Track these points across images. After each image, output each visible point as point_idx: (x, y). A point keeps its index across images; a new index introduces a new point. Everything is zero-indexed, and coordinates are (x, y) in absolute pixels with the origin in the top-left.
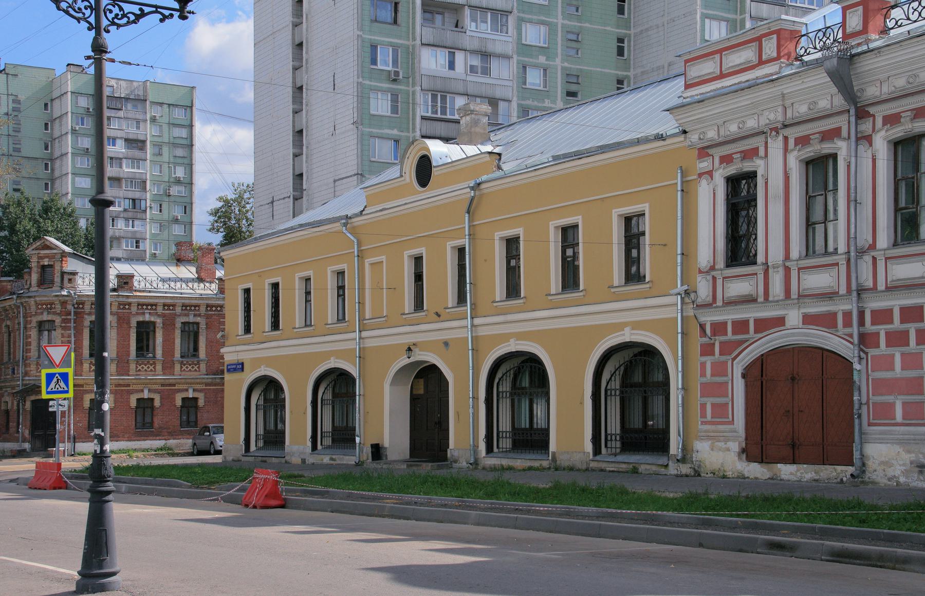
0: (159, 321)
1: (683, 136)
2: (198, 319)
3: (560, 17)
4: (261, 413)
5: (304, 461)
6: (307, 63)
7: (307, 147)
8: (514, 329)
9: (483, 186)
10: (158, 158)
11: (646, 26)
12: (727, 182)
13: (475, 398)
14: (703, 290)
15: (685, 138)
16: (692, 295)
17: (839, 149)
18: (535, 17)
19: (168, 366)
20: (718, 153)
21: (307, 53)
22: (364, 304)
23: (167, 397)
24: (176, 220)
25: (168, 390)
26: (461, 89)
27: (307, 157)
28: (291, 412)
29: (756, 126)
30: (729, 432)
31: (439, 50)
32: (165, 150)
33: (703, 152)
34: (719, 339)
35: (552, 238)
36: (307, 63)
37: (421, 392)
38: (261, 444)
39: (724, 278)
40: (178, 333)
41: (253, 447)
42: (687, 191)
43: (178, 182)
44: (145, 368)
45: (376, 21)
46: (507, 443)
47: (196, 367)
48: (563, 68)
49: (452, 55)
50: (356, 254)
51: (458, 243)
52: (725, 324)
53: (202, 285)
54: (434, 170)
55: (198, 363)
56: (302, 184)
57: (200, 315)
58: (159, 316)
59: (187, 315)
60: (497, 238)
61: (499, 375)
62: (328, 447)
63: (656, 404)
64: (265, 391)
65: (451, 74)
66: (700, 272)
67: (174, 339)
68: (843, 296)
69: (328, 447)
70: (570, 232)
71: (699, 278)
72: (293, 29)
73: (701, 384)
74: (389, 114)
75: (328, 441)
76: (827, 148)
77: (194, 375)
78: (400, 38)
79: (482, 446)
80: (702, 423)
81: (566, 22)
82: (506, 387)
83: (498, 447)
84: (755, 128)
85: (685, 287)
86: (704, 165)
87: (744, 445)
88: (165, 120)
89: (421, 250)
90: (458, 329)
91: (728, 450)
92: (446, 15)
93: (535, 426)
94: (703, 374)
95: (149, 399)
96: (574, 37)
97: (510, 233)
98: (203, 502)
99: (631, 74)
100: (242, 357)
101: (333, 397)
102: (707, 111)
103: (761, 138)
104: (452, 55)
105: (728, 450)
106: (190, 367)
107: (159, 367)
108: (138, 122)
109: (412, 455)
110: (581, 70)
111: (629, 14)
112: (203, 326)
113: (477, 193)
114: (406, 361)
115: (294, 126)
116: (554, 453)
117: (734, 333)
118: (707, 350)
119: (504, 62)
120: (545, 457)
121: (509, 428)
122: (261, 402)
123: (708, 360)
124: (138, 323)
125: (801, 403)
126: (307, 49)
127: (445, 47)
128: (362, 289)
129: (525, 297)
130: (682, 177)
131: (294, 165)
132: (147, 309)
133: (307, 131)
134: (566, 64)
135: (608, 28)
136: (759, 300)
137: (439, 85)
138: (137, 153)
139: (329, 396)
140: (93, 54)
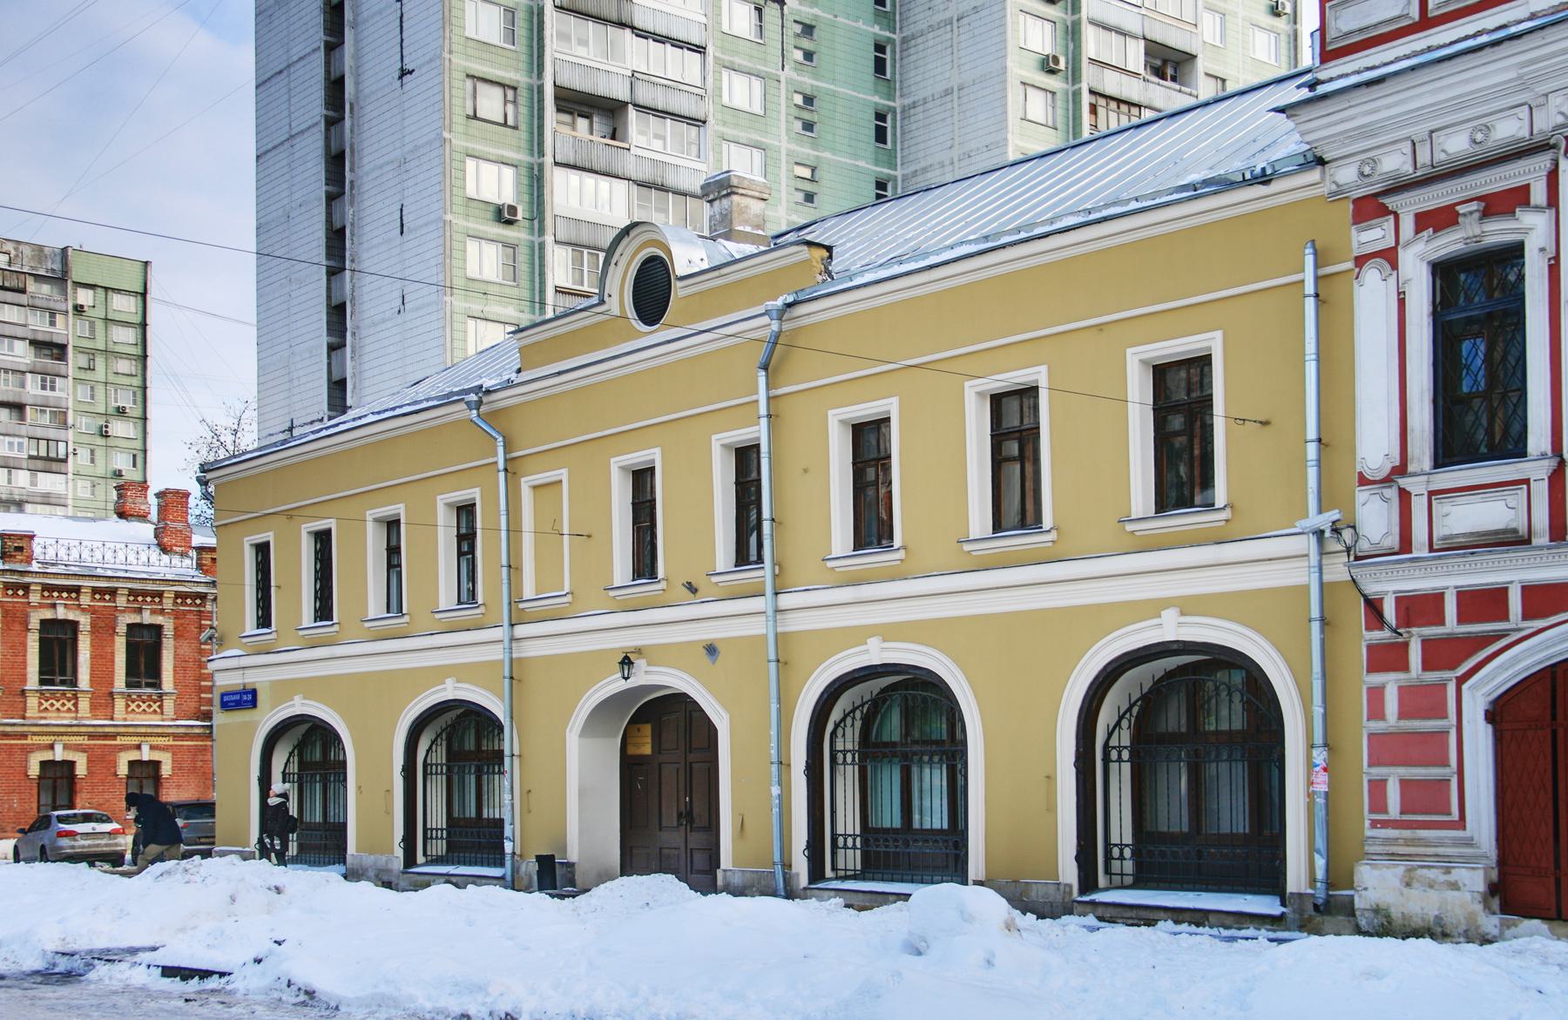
0: (84, 621)
1: (1318, 170)
2: (159, 620)
3: (784, 138)
6: (352, 188)
7: (354, 334)
8: (866, 619)
9: (735, 198)
10: (88, 375)
11: (923, 164)
12: (1434, 275)
13: (784, 764)
14: (1375, 518)
15: (1323, 173)
16: (1347, 535)
17: (1527, 231)
18: (492, 150)
19: (104, 700)
20: (1409, 206)
21: (352, 170)
22: (519, 569)
23: (102, 760)
24: (121, 412)
25: (102, 745)
27: (353, 352)
28: (389, 792)
29: (1525, 133)
30: (1455, 845)
32: (100, 362)
33: (1369, 208)
34: (1429, 634)
35: (441, 520)
36: (352, 188)
37: (647, 750)
38: (439, 847)
39: (1431, 494)
40: (120, 644)
42: (1331, 299)
44: (58, 705)
45: (475, 117)
46: (852, 859)
47: (155, 706)
50: (501, 465)
51: (742, 436)
52: (1437, 598)
53: (165, 558)
54: (677, 287)
55: (161, 696)
56: (344, 399)
57: (162, 612)
58: (84, 610)
59: (139, 611)
60: (369, 518)
61: (836, 715)
64: (301, 747)
66: (1363, 481)
67: (113, 654)
68: (1541, 548)
70: (1012, 405)
71: (1362, 495)
72: (327, 130)
74: (499, 280)
76: (1497, 232)
77: (155, 720)
80: (1374, 824)
81: (793, 147)
82: (849, 740)
84: (1522, 140)
85: (1334, 515)
86: (1376, 235)
87: (1494, 875)
88: (99, 312)
89: (651, 455)
90: (741, 621)
91: (1454, 886)
92: (595, 119)
93: (916, 825)
94: (1377, 712)
95: (64, 762)
96: (807, 173)
97: (866, 411)
99: (899, 173)
100: (251, 679)
101: (448, 760)
103: (1542, 162)
105: (1454, 886)
106: (144, 706)
107: (84, 704)
108: (53, 315)
110: (816, 17)
111: (894, 142)
112: (169, 630)
113: (785, 327)
114: (622, 685)
115: (329, 297)
117: (1462, 619)
118: (1387, 658)
123: (1391, 683)
124: (43, 622)
126: (352, 164)
128: (514, 530)
129: (904, 547)
130: (1317, 266)
131: (329, 364)
132: (60, 597)
133: (353, 305)
135: (862, 164)
136: (1535, 542)
138: (49, 363)
139: (440, 756)
140: (1141, 71)
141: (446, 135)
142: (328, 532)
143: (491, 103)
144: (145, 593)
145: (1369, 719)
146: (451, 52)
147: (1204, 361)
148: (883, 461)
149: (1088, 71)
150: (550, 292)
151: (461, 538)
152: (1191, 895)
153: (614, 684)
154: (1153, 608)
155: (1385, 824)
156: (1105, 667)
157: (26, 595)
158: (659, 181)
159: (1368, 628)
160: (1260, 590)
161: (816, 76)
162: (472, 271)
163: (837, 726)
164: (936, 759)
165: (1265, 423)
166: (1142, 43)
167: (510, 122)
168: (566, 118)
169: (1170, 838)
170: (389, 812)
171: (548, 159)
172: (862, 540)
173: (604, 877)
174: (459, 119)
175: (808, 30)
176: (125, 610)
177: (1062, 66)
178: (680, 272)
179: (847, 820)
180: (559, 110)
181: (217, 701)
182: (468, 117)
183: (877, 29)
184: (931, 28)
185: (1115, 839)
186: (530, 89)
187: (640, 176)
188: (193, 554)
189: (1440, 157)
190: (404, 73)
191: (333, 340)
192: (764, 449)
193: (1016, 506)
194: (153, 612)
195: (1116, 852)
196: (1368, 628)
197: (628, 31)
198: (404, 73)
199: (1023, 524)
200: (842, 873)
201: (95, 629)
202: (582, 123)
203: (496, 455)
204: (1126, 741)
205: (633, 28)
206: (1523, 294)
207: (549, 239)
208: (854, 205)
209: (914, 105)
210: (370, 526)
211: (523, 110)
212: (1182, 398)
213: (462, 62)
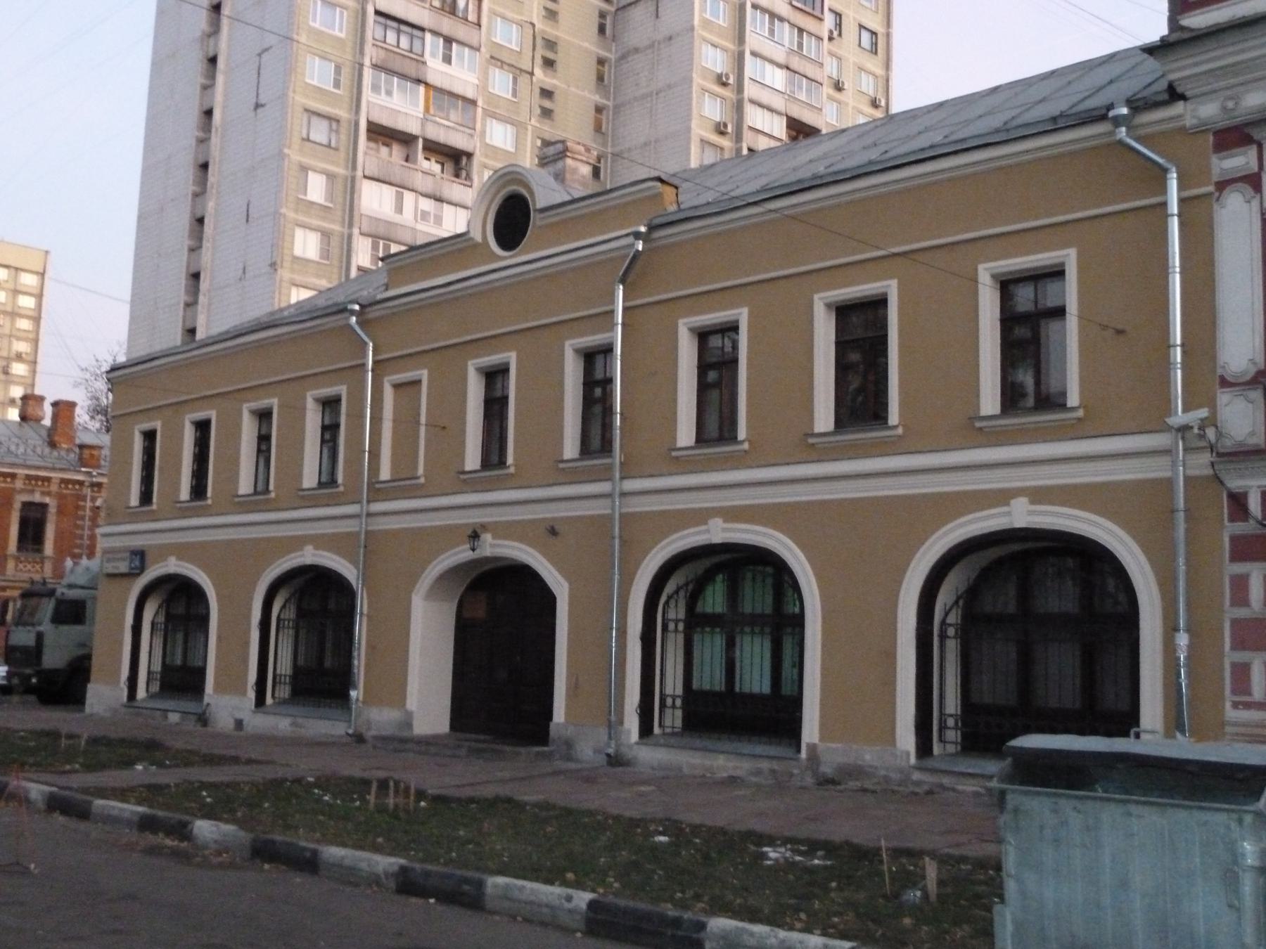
2: (47, 500)
4: (158, 642)
5: (239, 724)
8: (722, 504)
31: (385, 187)
38: (155, 687)
40: (377, 507)
41: (141, 693)
43: (19, 357)
46: (675, 718)
49: (400, 198)
57: (49, 494)
61: (670, 588)
62: (284, 702)
64: (167, 603)
65: (397, 218)
66: (1224, 383)
67: (9, 525)
69: (284, 702)
71: (1223, 397)
72: (193, 200)
73: (1235, 622)
75: (285, 692)
79: (632, 723)
80: (1236, 705)
82: (678, 612)
83: (660, 725)
85: (1203, 413)
90: (582, 500)
93: (737, 690)
94: (1240, 597)
102: (1196, 64)
104: (400, 198)
106: (29, 567)
109: (453, 727)
112: (52, 510)
116: (812, 748)
120: (789, 752)
121: (679, 691)
122: (161, 619)
127: (390, 184)
135: (586, 45)
137: (381, 230)
139: (291, 614)
141: (286, 151)
142: (503, 370)
143: (320, 132)
144: (37, 478)
145: (1232, 605)
146: (294, 92)
147: (880, 302)
151: (324, 428)
153: (462, 554)
154: (1003, 497)
155: (1248, 706)
156: (335, 572)
157: (13, 482)
158: (438, 194)
159: (1232, 520)
160: (675, 401)
162: (298, 252)
163: (670, 597)
164: (757, 630)
165: (1120, 332)
166: (1256, 169)
167: (333, 144)
168: (372, 145)
169: (10, 343)
171: (359, 173)
174: (296, 140)
175: (547, 93)
176: (22, 491)
177: (729, 129)
178: (540, 204)
179: (672, 682)
180: (369, 139)
181: (1030, 484)
182: (303, 139)
184: (636, 99)
185: (669, 691)
186: (350, 122)
187: (424, 190)
188: (77, 450)
189: (908, 95)
190: (258, 106)
191: (201, 135)
192: (618, 350)
193: (862, 401)
194: (43, 493)
195: (669, 701)
196: (1232, 520)
197: (420, 189)
198: (258, 106)
200: (668, 730)
201: (61, 511)
202: (384, 150)
203: (1163, 189)
204: (682, 615)
205: (426, 84)
207: (356, 231)
208: (376, 176)
210: (1073, 399)
211: (343, 137)
212: (861, 330)
213: (300, 99)
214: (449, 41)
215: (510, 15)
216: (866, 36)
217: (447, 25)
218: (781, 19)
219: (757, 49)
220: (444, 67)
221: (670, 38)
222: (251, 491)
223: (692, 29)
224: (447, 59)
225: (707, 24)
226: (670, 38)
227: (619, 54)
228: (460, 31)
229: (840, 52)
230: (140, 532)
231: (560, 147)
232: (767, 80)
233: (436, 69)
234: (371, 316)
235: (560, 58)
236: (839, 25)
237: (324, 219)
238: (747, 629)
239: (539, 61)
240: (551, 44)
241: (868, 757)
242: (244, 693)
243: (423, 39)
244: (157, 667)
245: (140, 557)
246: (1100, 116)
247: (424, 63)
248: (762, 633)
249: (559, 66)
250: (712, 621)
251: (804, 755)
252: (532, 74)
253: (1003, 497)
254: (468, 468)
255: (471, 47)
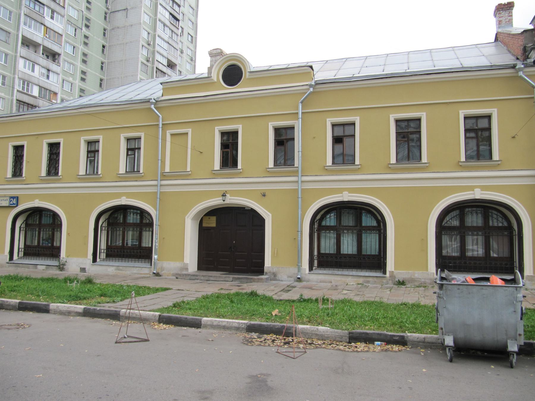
4: (23, 234)
26: (37, 82)
28: (68, 234)
38: (21, 254)
40: (164, 182)
41: (15, 257)
48: (79, 86)
62: (104, 260)
63: (57, 234)
65: (32, 74)
70: (351, 158)
75: (103, 256)
78: (9, 50)
90: (284, 182)
93: (342, 253)
98: (108, 312)
116: (392, 272)
119: (56, 76)
122: (24, 226)
125: (478, 237)
134: (80, 84)
135: (99, 4)
137: (26, 78)
139: (105, 225)
148: (58, 154)
149: (156, 63)
150: (15, 91)
152: (6, 240)
156: (448, 206)
161: (88, 50)
170: (425, 241)
171: (18, 54)
172: (49, 173)
173: (499, 23)
175: (86, 37)
181: (346, 188)
183: (103, 42)
199: (285, 164)
205: (45, 25)
206: (103, 318)
209: (111, 62)
214: (53, 12)
215: (75, 6)
216: (190, 37)
217: (53, 5)
218: (167, 26)
219: (160, 34)
220: (51, 20)
221: (132, 26)
222: (84, 173)
223: (140, 24)
224: (52, 18)
225: (144, 22)
226: (132, 26)
227: (111, 28)
228: (57, 8)
229: (182, 41)
230: (16, 188)
231: (219, 51)
232: (161, 45)
233: (48, 21)
234: (159, 106)
235: (91, 25)
236: (183, 32)
237: (4, 70)
238: (345, 231)
239: (84, 25)
240: (88, 20)
241: (416, 275)
242: (86, 256)
243: (44, 8)
244: (22, 245)
245: (15, 200)
246: (148, 101)
247: (44, 17)
248: (353, 233)
249: (91, 28)
250: (329, 228)
251: (388, 274)
252: (82, 29)
253: (472, 188)
254: (462, 160)
255: (61, 15)
